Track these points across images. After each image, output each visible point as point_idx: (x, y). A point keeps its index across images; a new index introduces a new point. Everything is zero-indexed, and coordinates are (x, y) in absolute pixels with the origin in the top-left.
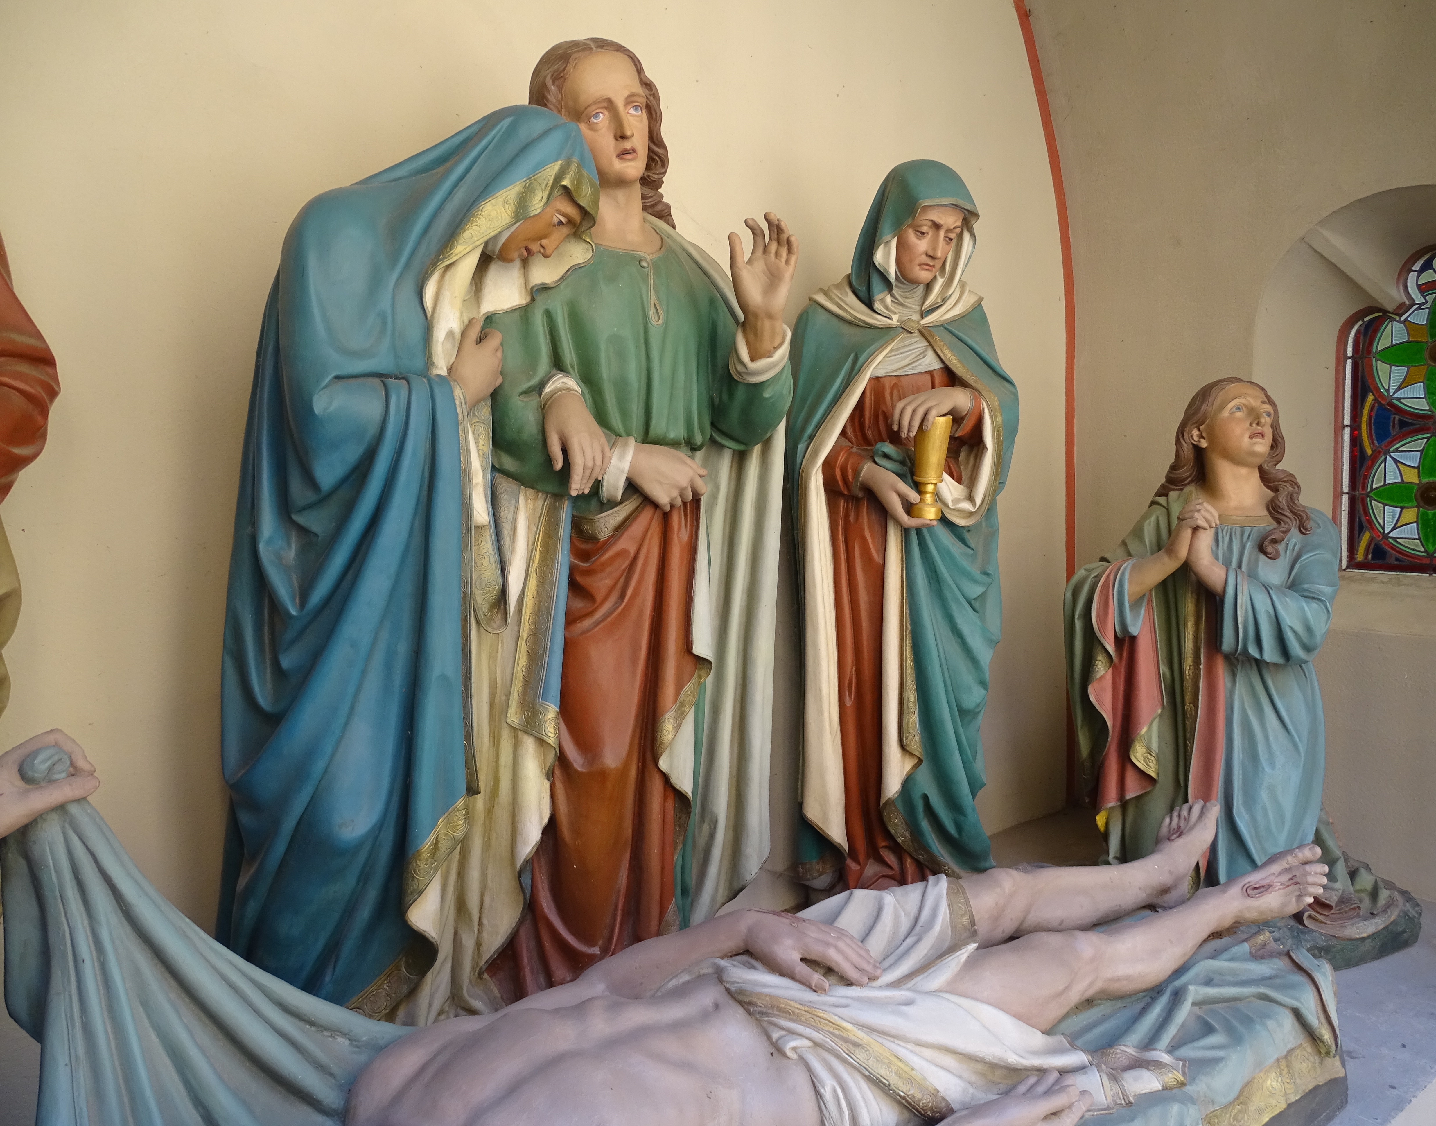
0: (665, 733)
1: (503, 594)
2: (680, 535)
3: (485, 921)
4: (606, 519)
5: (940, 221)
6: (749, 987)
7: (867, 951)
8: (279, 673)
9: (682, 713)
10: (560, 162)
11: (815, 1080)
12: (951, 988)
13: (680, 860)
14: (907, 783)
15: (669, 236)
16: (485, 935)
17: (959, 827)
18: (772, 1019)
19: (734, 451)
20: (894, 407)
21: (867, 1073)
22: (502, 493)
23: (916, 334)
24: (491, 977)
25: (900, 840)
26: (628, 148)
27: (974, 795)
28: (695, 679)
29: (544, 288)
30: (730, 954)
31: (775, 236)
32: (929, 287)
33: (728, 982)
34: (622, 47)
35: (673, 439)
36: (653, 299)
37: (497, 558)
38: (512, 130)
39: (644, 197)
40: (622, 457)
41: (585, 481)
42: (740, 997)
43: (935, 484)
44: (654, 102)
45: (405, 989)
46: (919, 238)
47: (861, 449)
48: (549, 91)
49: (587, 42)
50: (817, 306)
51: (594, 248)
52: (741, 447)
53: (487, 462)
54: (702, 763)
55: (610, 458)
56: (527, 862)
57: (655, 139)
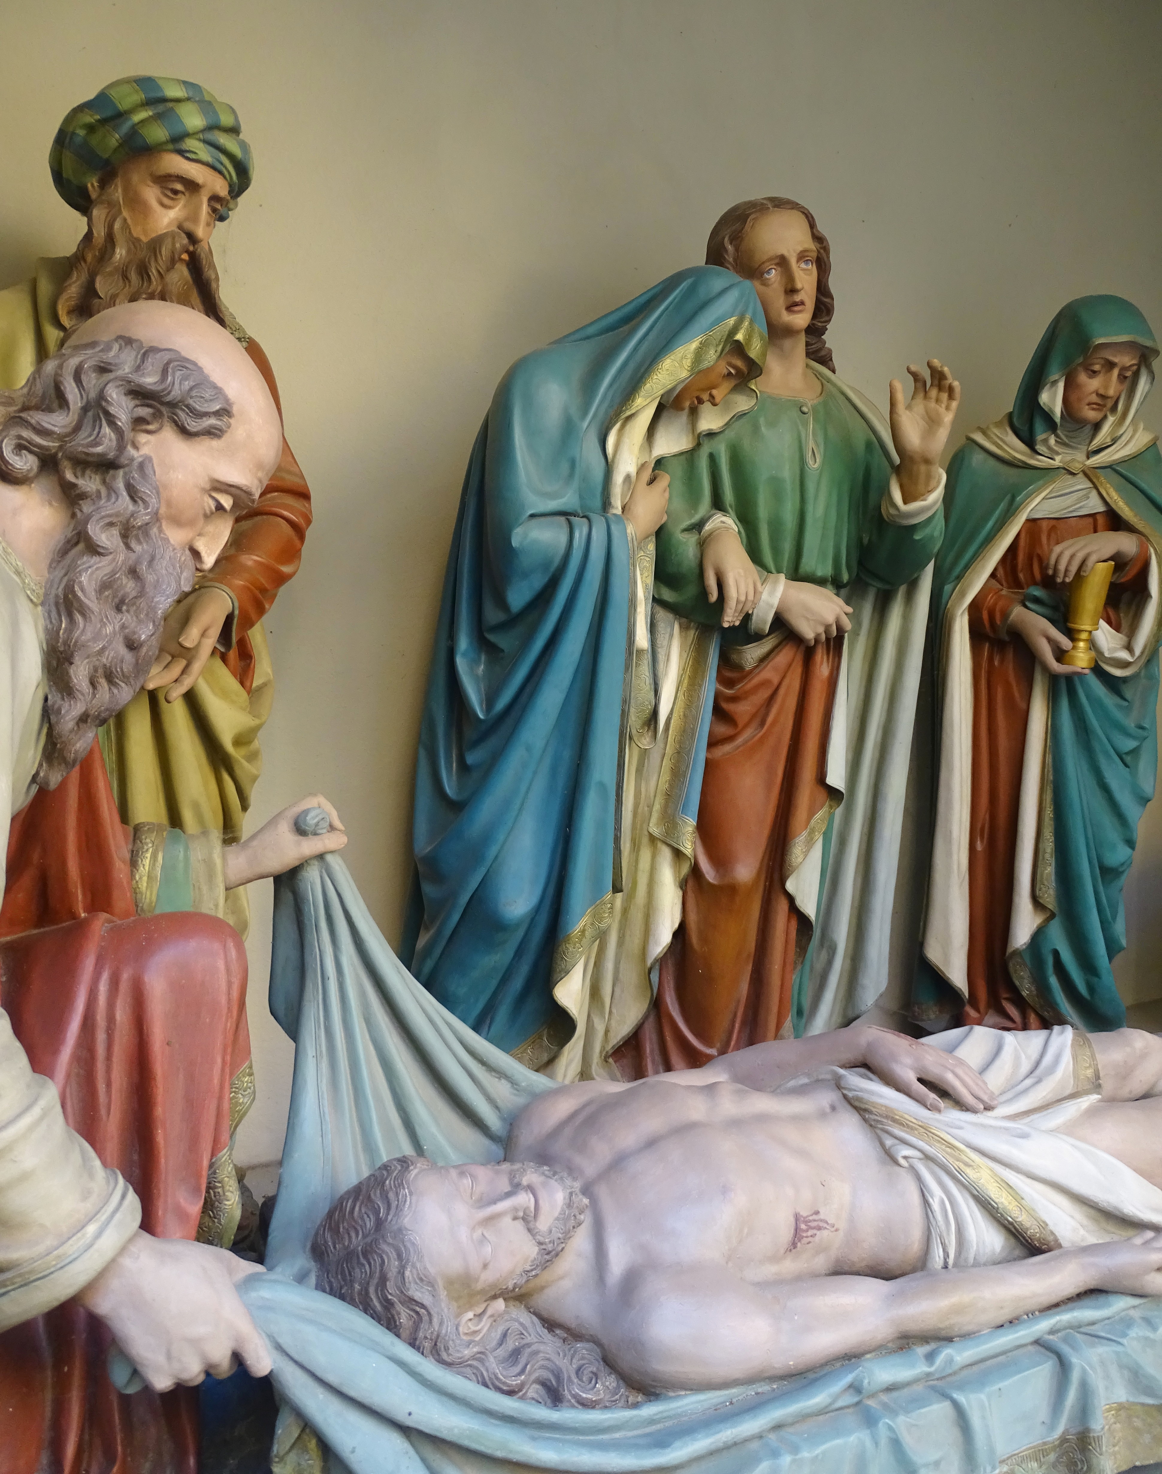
0: (794, 856)
1: (655, 714)
2: (822, 668)
3: (614, 1011)
5: (1116, 360)
6: (865, 1096)
7: (985, 1083)
8: (464, 768)
9: (812, 839)
11: (924, 1189)
12: (1069, 1130)
13: (798, 980)
14: (1038, 936)
15: (829, 381)
16: (613, 1023)
17: (1091, 988)
18: (886, 1127)
19: (879, 590)
20: (1051, 551)
21: (976, 1193)
22: (659, 621)
23: (1081, 475)
24: (615, 1062)
25: (1025, 993)
26: (797, 300)
27: (1110, 958)
28: (825, 809)
29: (711, 435)
30: (848, 1066)
31: (936, 382)
32: (1097, 426)
33: (845, 1088)
34: (798, 204)
36: (811, 444)
37: (652, 681)
38: (692, 290)
39: (807, 344)
40: (772, 593)
41: (737, 614)
42: (857, 1104)
43: (1090, 632)
44: (824, 255)
45: (545, 1057)
46: (1090, 377)
47: (1012, 592)
48: (726, 251)
49: (765, 202)
50: (974, 444)
51: (759, 395)
52: (887, 587)
53: (649, 593)
54: (825, 891)
55: (761, 593)
56: (657, 961)
57: (822, 290)
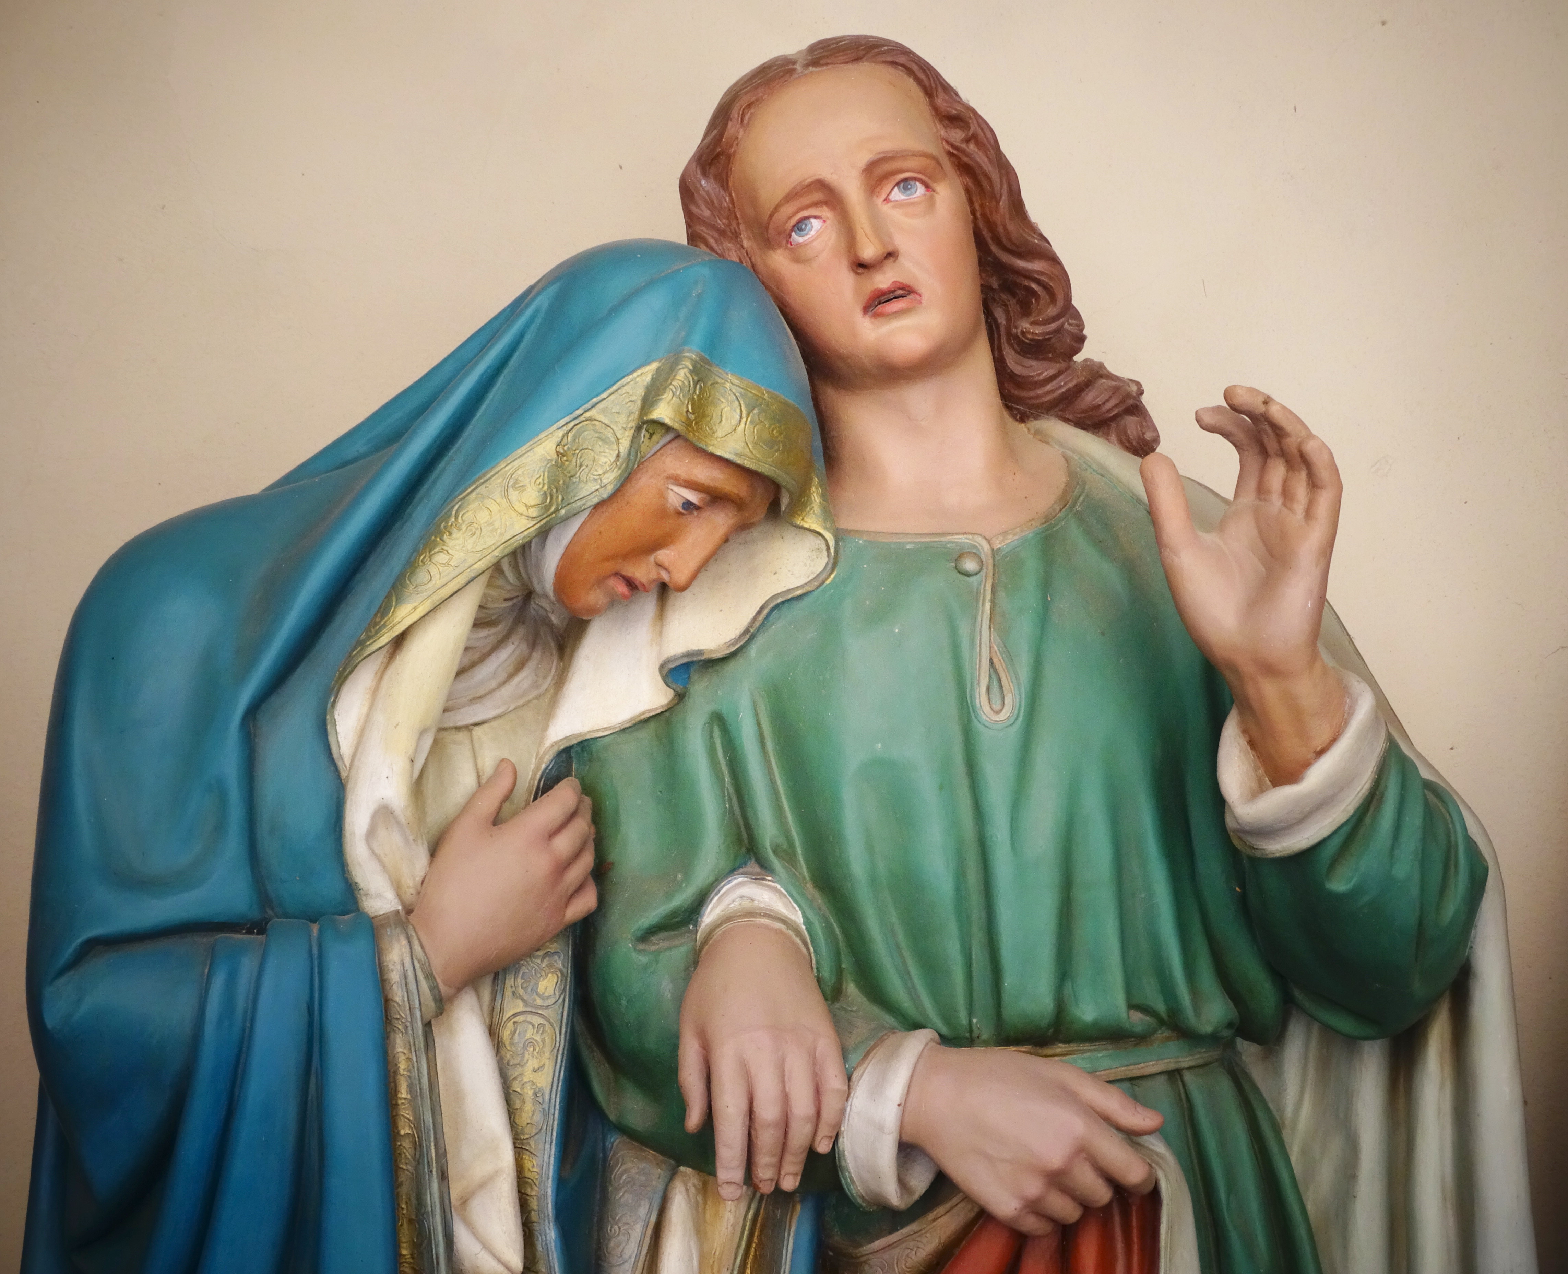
4: (886, 1256)
10: (654, 366)
35: (1095, 1024)
